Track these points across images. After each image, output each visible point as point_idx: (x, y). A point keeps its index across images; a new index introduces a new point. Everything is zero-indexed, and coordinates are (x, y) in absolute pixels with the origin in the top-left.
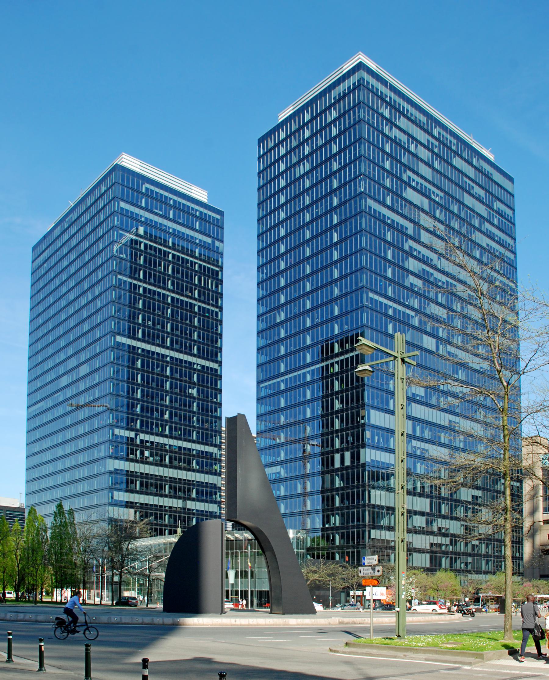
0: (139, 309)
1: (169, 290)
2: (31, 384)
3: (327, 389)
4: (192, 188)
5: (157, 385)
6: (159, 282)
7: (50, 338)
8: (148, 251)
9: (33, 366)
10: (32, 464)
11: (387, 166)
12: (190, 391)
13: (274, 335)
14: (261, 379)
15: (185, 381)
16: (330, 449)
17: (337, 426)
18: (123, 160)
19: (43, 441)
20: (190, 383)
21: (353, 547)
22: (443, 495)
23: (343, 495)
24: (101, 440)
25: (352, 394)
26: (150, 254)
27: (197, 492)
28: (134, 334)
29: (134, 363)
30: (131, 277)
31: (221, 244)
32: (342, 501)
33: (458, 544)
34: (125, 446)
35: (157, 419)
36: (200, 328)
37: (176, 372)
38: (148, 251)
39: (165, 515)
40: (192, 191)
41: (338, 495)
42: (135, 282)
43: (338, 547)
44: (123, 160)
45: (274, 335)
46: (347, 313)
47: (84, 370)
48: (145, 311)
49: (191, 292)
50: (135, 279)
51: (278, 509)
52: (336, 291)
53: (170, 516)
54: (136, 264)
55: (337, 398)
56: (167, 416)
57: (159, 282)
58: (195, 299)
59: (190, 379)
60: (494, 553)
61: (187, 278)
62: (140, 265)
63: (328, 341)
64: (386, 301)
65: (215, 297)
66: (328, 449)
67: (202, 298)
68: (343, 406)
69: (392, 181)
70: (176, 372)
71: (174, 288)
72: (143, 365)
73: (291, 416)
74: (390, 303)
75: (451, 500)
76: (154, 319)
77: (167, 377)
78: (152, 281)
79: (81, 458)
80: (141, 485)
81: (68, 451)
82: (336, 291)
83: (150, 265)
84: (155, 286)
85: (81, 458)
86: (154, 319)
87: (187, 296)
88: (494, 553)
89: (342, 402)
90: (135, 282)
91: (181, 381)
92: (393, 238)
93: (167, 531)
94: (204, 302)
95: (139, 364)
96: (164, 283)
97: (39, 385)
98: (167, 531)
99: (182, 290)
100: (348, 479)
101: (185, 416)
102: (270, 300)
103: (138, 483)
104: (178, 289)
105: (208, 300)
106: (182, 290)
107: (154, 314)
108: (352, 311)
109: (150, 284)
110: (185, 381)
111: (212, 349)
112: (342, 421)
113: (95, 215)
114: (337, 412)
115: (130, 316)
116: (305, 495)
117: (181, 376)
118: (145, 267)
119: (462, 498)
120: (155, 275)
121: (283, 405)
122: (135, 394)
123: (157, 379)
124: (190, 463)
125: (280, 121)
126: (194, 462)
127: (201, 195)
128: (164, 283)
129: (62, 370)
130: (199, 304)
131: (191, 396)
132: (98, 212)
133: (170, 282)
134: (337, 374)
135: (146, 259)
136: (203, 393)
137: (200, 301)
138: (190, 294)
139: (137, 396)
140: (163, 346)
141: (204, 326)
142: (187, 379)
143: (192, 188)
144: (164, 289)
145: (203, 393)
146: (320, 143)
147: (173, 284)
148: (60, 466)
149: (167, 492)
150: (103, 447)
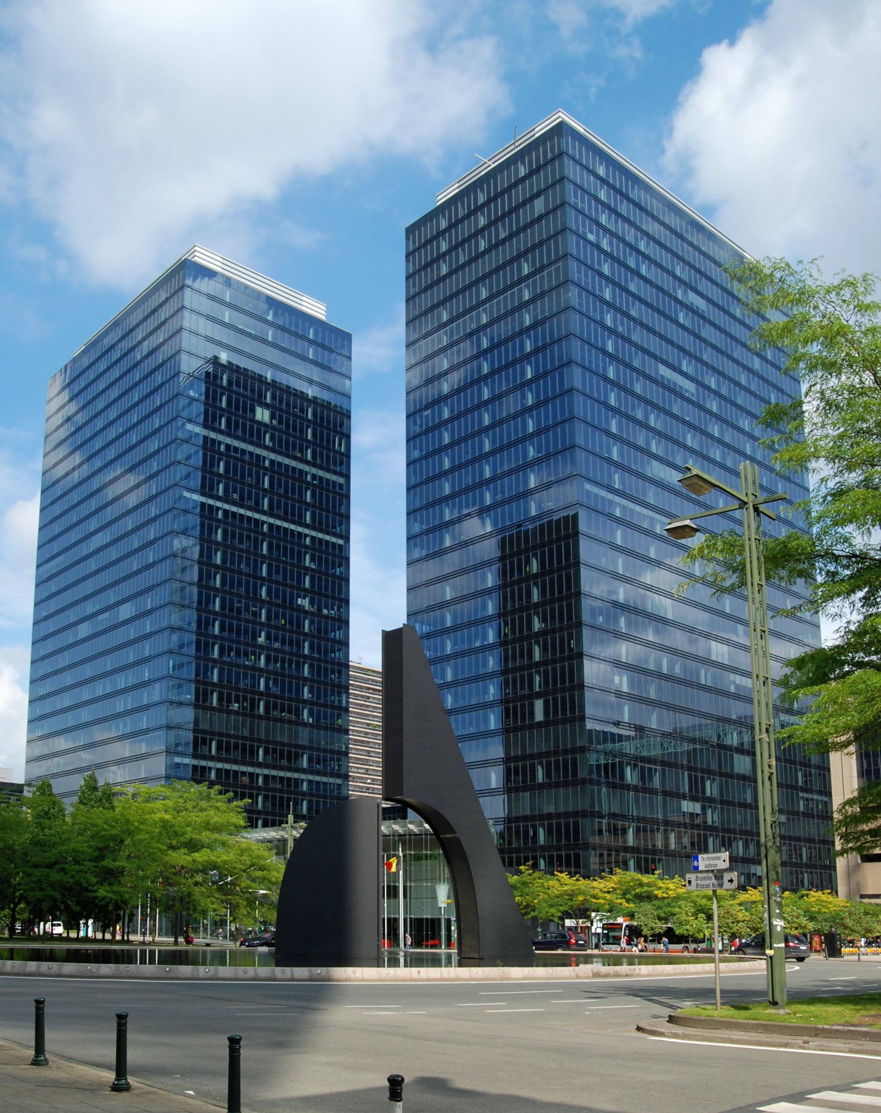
0: (219, 475)
1: (266, 448)
2: (42, 549)
3: (520, 599)
4: (303, 298)
5: (247, 592)
6: (251, 435)
7: (74, 517)
8: (234, 388)
9: (48, 521)
10: (39, 713)
11: (606, 270)
12: (300, 601)
13: (434, 518)
14: (413, 482)
15: (292, 587)
16: (527, 691)
17: (537, 657)
18: (196, 253)
19: (59, 657)
20: (299, 589)
21: (568, 847)
22: (710, 822)
23: (549, 764)
24: (153, 725)
25: (560, 578)
26: (238, 393)
27: (310, 760)
28: (211, 488)
29: (210, 557)
30: (203, 494)
31: (347, 382)
32: (548, 774)
33: (734, 844)
34: (193, 686)
35: (247, 644)
36: (314, 506)
37: (278, 572)
38: (234, 388)
39: (259, 701)
40: (303, 303)
41: (541, 764)
42: (211, 502)
43: (542, 847)
44: (196, 253)
45: (434, 518)
46: (547, 429)
47: (126, 611)
48: (224, 592)
49: (301, 451)
50: (214, 429)
51: (442, 701)
52: (531, 452)
53: (266, 798)
54: (215, 407)
55: (537, 613)
56: (261, 640)
57: (251, 435)
58: (308, 463)
59: (299, 582)
60: (790, 858)
61: (292, 579)
62: (222, 409)
63: (520, 526)
64: (610, 496)
65: (340, 462)
66: (523, 693)
67: (319, 461)
68: (546, 625)
69: (614, 293)
70: (278, 572)
71: (274, 444)
72: (223, 607)
73: (463, 641)
74: (617, 499)
75: (723, 830)
76: (242, 490)
77: (263, 579)
78: (240, 433)
79: (122, 681)
80: (219, 748)
81: (99, 692)
82: (531, 452)
83: (237, 408)
84: (244, 440)
85: (122, 681)
86: (242, 490)
87: (295, 458)
88: (790, 858)
89: (544, 620)
90: (211, 502)
91: (285, 585)
92: (618, 376)
93: (260, 822)
94: (321, 468)
95: (218, 559)
96: (259, 437)
97: (52, 629)
98: (260, 822)
99: (287, 449)
100: (553, 618)
101: (292, 551)
102: (427, 440)
103: (214, 744)
104: (280, 446)
105: (328, 464)
106: (287, 449)
107: (243, 483)
108: (555, 398)
109: (236, 438)
110: (292, 587)
111: (334, 508)
112: (545, 649)
113: (147, 417)
114: (537, 634)
115: (200, 602)
116: (484, 649)
117: (285, 578)
118: (230, 412)
119: (736, 770)
120: (244, 425)
121: (449, 678)
122: (211, 605)
123: (248, 582)
124: (298, 713)
125: (439, 203)
126: (306, 711)
127: (316, 309)
128: (259, 437)
129: (93, 524)
130: (314, 533)
131: (300, 609)
132: (152, 393)
133: (267, 436)
134: (535, 576)
135: (230, 392)
136: (321, 456)
137: (314, 465)
138: (299, 455)
139: (214, 631)
140: (257, 509)
141: (321, 503)
142: (295, 583)
143: (303, 298)
144: (259, 446)
145: (321, 456)
146: (502, 235)
147: (272, 438)
148: (86, 694)
149: (261, 759)
150: (157, 686)
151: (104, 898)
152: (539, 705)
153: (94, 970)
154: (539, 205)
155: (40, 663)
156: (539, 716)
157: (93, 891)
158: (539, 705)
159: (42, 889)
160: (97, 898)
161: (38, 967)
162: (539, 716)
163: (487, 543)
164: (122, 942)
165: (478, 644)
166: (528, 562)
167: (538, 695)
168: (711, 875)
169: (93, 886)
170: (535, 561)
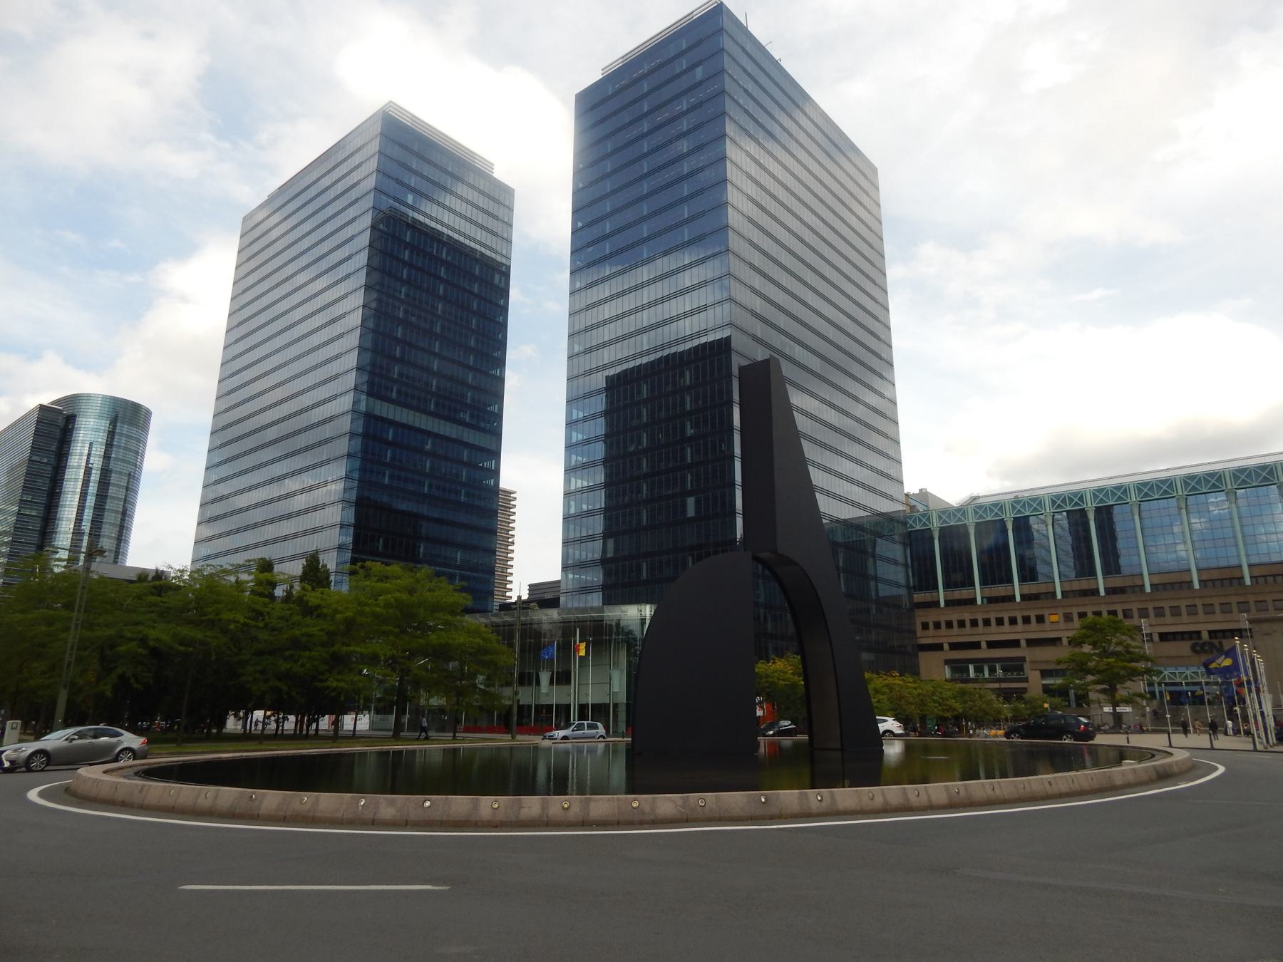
114: (690, 439)
151: (335, 689)
152: (691, 502)
153: (647, 808)
154: (699, 73)
155: (217, 452)
156: (691, 512)
157: (321, 681)
158: (691, 502)
159: (266, 681)
160: (328, 688)
161: (544, 807)
162: (691, 512)
163: (333, 487)
164: (296, 737)
165: (632, 448)
166: (682, 375)
167: (690, 494)
168: (1185, 647)
169: (322, 674)
170: (688, 373)
